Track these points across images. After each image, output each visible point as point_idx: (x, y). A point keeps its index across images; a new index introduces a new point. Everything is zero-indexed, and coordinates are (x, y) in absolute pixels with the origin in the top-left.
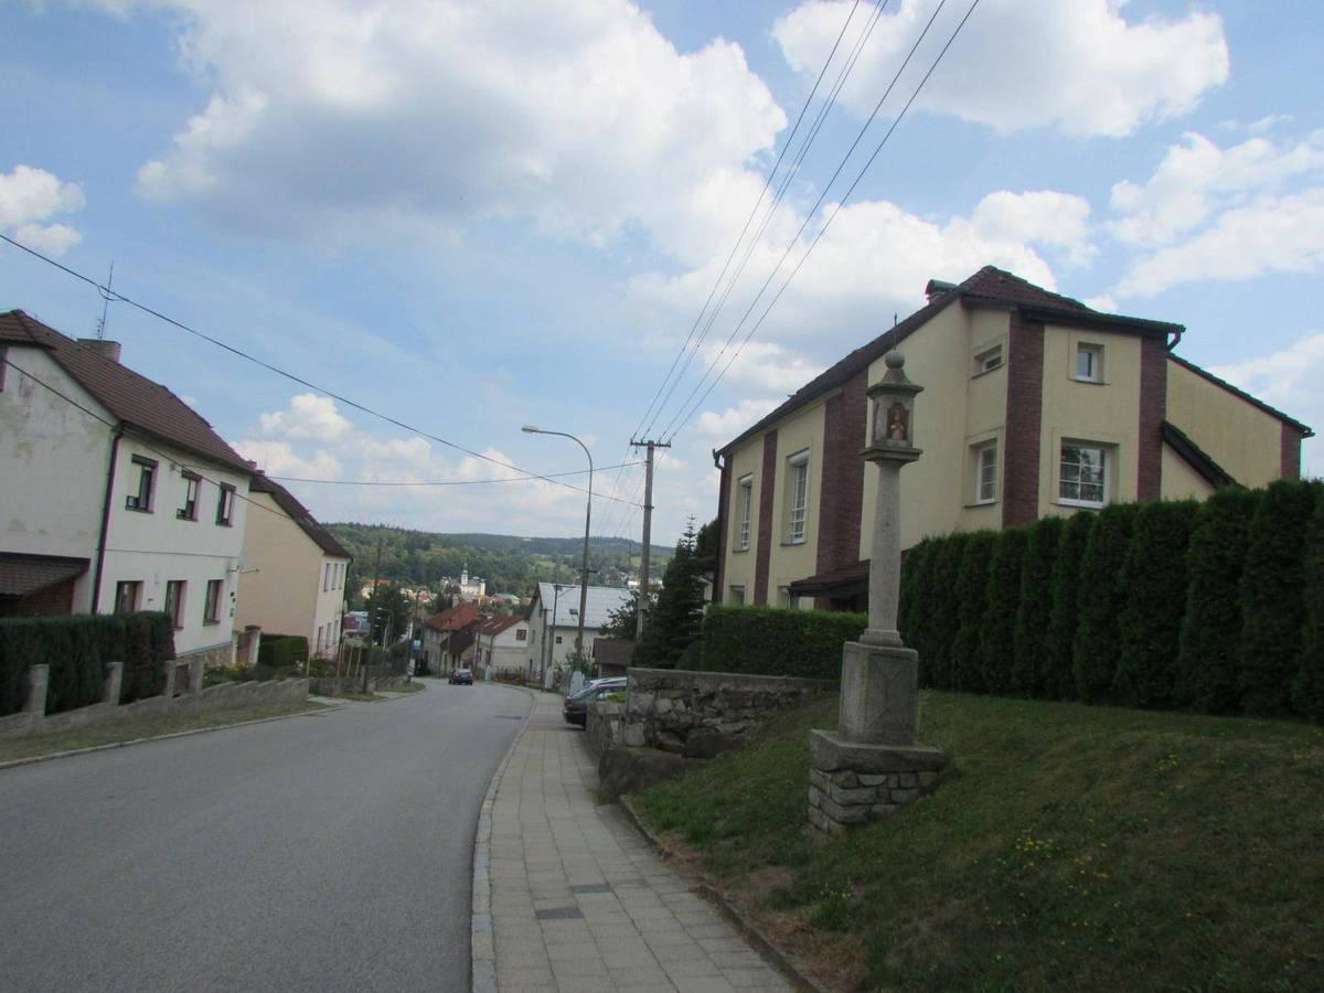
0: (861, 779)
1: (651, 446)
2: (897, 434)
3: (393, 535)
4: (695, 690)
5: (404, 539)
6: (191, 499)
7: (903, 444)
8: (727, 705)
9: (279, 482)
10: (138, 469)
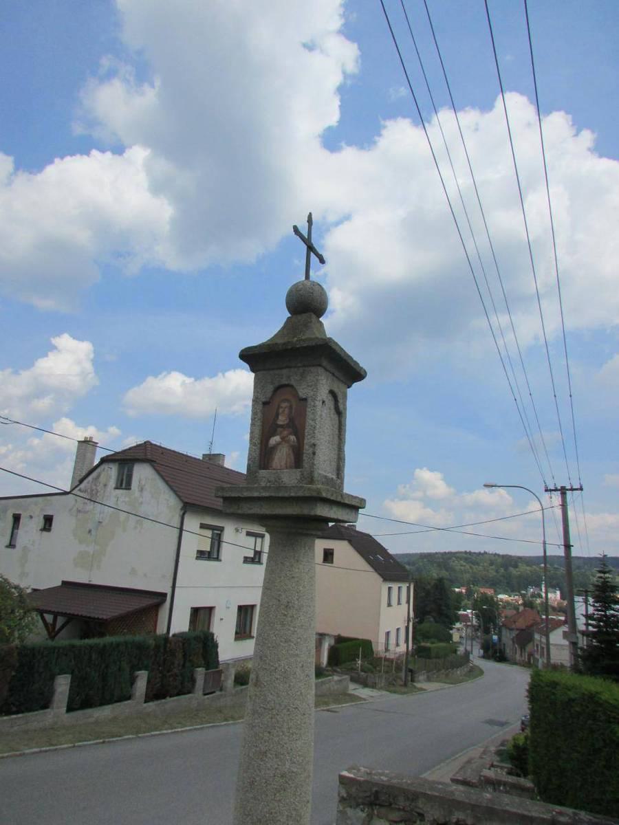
1: (563, 491)
2: (282, 456)
3: (493, 558)
5: (500, 560)
6: (258, 549)
7: (290, 478)
10: (209, 533)
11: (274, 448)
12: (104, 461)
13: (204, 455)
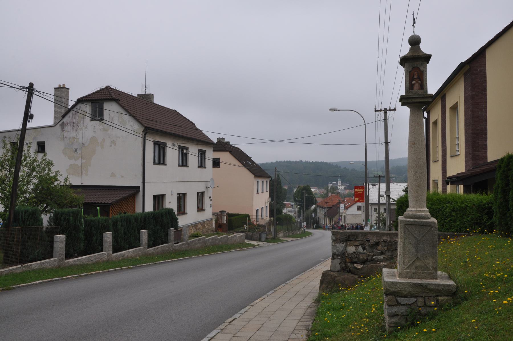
0: (399, 301)
1: (385, 111)
2: (416, 87)
4: (367, 241)
7: (421, 92)
8: (386, 248)
9: (237, 146)
12: (80, 101)
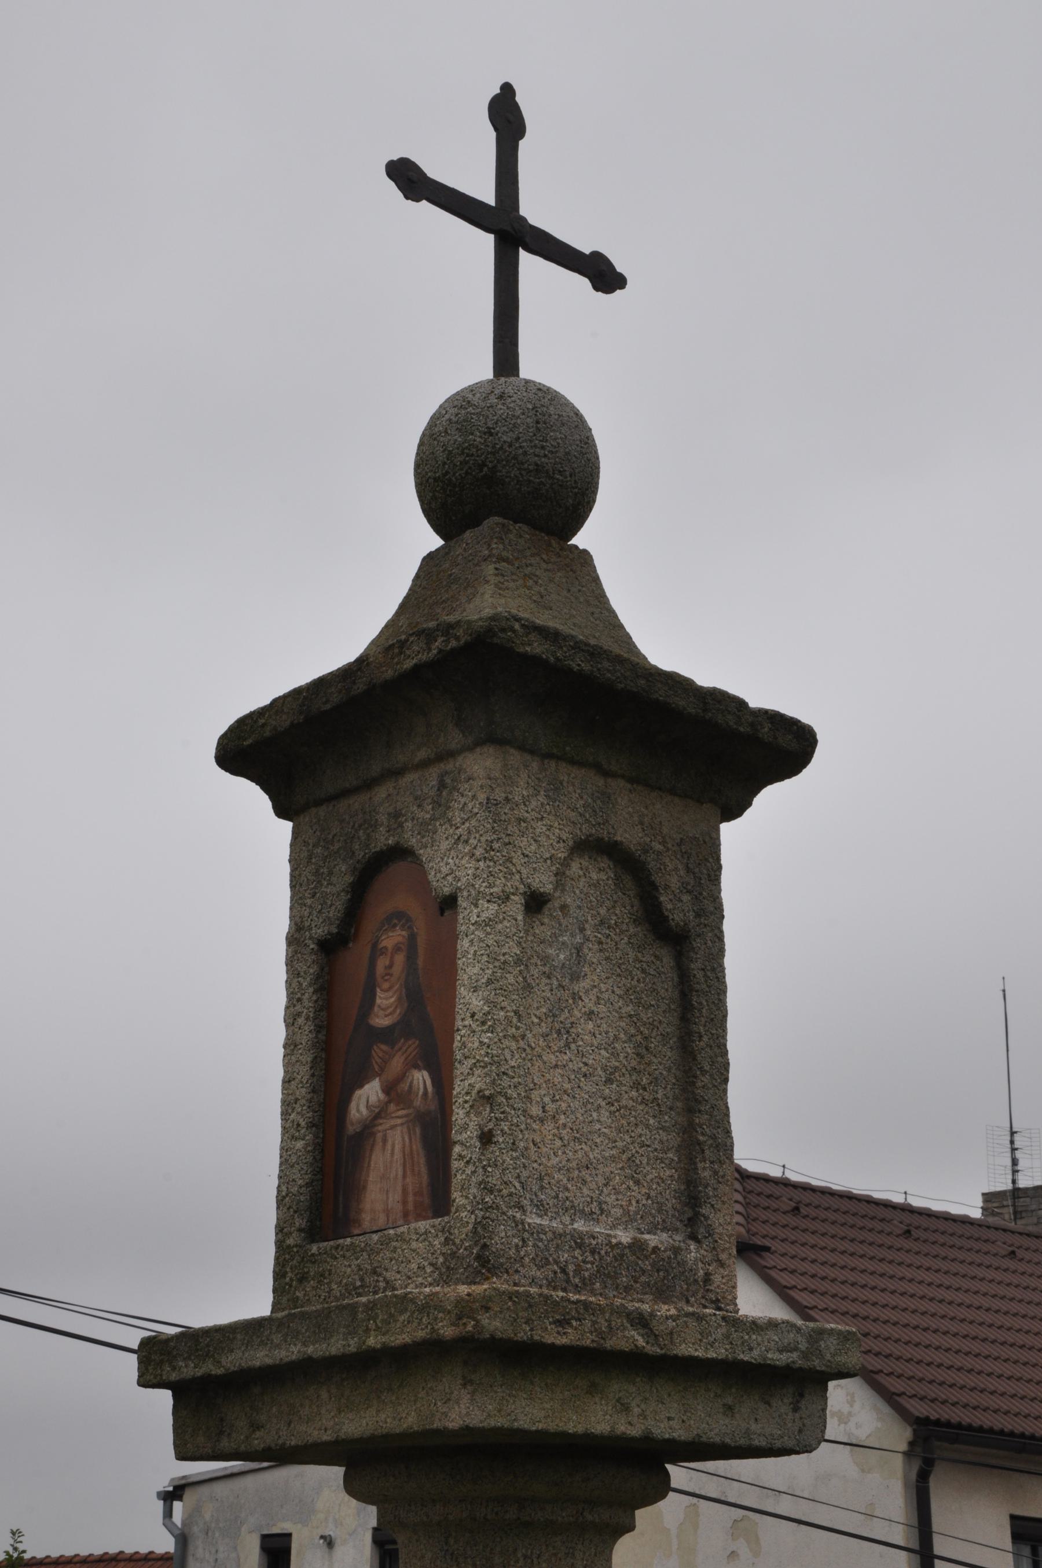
11: (367, 1131)
13: (988, 1197)
